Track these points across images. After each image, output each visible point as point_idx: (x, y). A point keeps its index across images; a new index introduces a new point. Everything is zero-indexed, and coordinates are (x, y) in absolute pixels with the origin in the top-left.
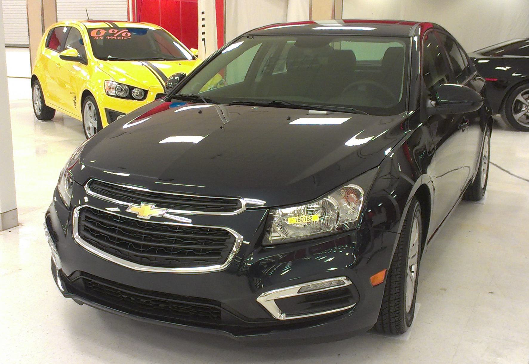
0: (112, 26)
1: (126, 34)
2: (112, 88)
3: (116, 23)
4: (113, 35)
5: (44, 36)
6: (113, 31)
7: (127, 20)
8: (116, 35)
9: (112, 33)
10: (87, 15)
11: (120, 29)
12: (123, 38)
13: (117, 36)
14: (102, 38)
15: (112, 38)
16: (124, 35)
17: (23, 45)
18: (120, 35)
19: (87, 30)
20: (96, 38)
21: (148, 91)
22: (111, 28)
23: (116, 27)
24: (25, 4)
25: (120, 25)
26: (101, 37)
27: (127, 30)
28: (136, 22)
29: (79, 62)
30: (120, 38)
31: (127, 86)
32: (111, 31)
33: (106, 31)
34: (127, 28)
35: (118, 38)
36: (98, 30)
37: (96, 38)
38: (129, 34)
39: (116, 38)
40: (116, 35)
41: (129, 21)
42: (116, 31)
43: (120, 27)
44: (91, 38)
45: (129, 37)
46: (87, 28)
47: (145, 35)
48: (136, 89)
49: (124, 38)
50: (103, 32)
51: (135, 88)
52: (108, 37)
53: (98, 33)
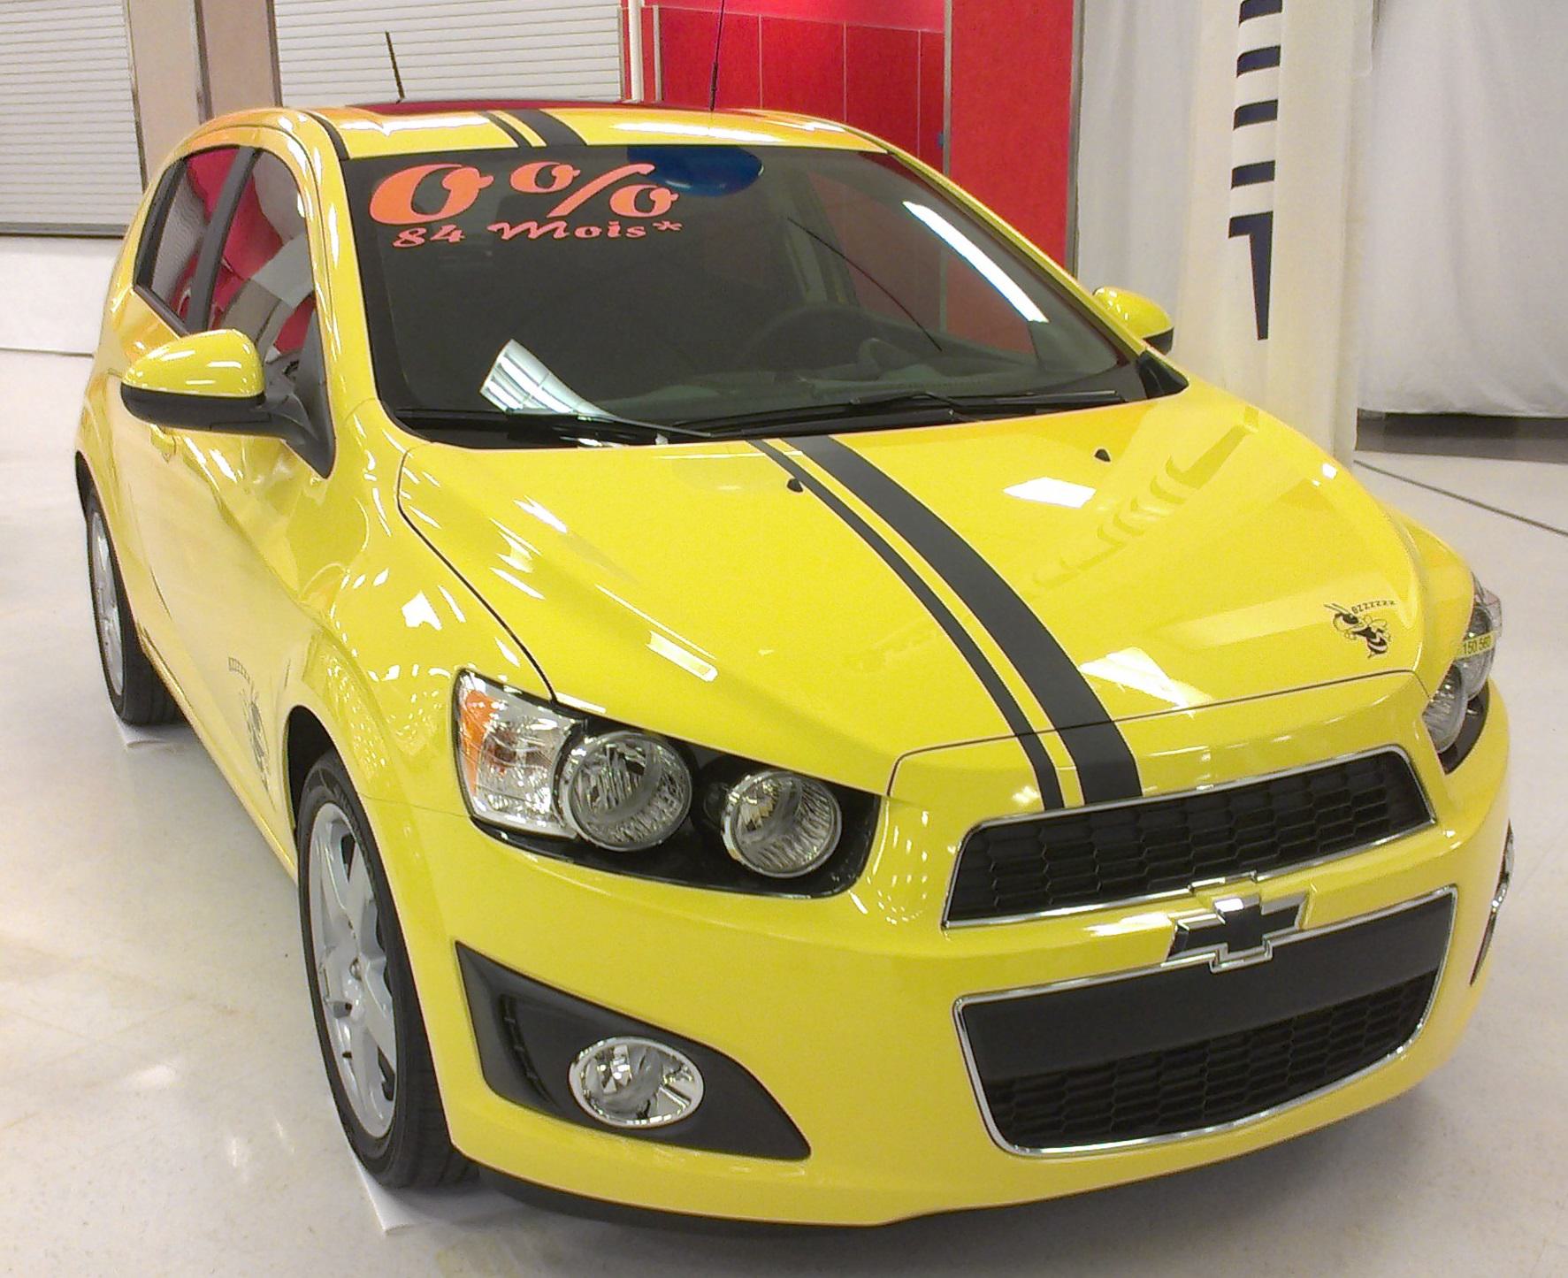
0: (535, 140)
1: (643, 202)
2: (521, 751)
3: (562, 115)
4: (537, 207)
5: (146, 192)
6: (544, 178)
7: (614, 93)
8: (564, 208)
9: (535, 189)
10: (394, 63)
11: (597, 158)
12: (614, 231)
13: (573, 220)
14: (456, 237)
15: (534, 234)
16: (623, 202)
17: (81, 226)
18: (597, 209)
19: (1166, 333)
20: (405, 235)
21: (885, 808)
22: (523, 153)
23: (565, 146)
24: (127, 85)
25: (596, 129)
26: (447, 229)
27: (646, 168)
28: (658, 106)
29: (283, 441)
30: (596, 231)
31: (680, 747)
32: (524, 179)
33: (489, 180)
34: (637, 153)
35: (580, 232)
36: (421, 172)
37: (405, 235)
38: (663, 199)
39: (560, 234)
40: (564, 208)
41: (627, 101)
42: (564, 174)
43: (590, 140)
44: (369, 235)
45: (660, 218)
46: (343, 158)
47: (741, 197)
48: (767, 774)
49: (623, 232)
50: (464, 187)
51: (755, 767)
52: (506, 226)
53: (428, 197)
